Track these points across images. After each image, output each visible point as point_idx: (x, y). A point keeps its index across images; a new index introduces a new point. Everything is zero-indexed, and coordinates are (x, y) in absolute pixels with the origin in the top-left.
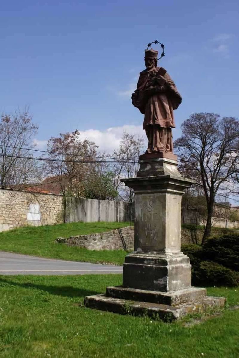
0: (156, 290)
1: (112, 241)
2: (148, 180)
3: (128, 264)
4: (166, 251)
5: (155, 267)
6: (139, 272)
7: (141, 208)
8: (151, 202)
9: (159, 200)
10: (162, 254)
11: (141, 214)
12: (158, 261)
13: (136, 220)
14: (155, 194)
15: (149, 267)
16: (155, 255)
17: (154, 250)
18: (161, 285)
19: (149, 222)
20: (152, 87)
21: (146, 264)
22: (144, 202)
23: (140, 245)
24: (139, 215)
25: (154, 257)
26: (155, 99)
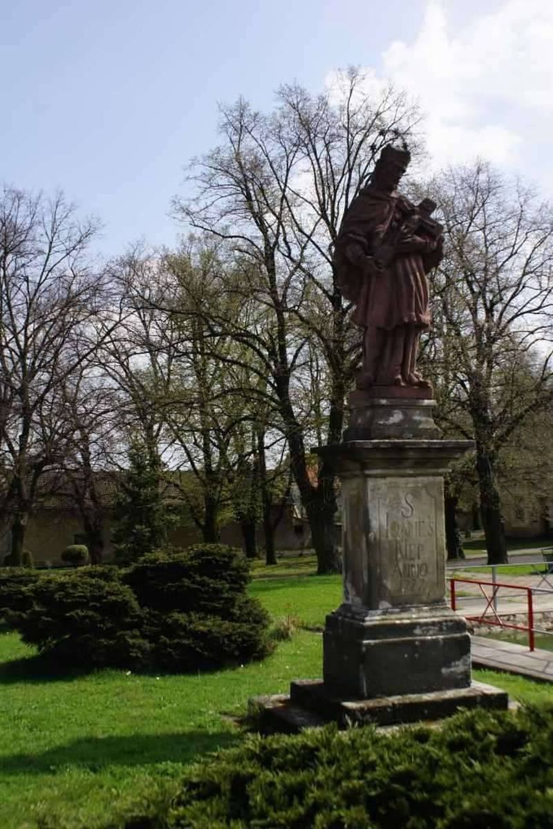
0: (449, 687)
3: (377, 641)
5: (444, 639)
6: (406, 656)
7: (386, 511)
9: (428, 493)
10: (443, 609)
11: (384, 523)
12: (446, 626)
14: (420, 479)
15: (428, 641)
17: (422, 603)
18: (459, 674)
19: (406, 541)
21: (421, 635)
22: (392, 496)
23: (387, 595)
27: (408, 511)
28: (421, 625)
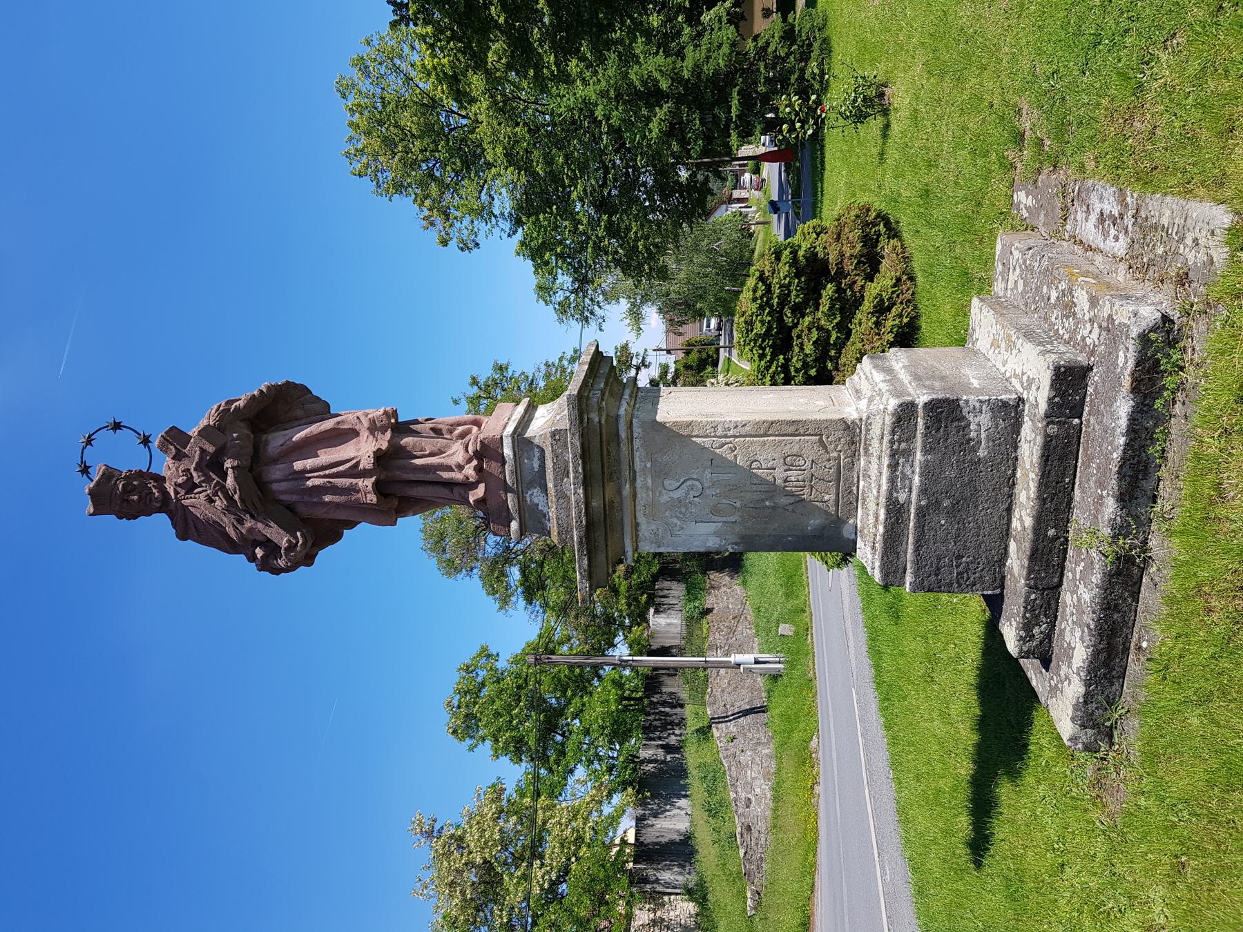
1: (748, 753)
2: (585, 490)
4: (854, 416)
5: (926, 452)
8: (666, 483)
10: (868, 430)
11: (712, 527)
13: (736, 544)
14: (638, 465)
16: (874, 460)
20: (230, 482)
25: (880, 465)
26: (276, 472)
27: (692, 488)
28: (890, 493)
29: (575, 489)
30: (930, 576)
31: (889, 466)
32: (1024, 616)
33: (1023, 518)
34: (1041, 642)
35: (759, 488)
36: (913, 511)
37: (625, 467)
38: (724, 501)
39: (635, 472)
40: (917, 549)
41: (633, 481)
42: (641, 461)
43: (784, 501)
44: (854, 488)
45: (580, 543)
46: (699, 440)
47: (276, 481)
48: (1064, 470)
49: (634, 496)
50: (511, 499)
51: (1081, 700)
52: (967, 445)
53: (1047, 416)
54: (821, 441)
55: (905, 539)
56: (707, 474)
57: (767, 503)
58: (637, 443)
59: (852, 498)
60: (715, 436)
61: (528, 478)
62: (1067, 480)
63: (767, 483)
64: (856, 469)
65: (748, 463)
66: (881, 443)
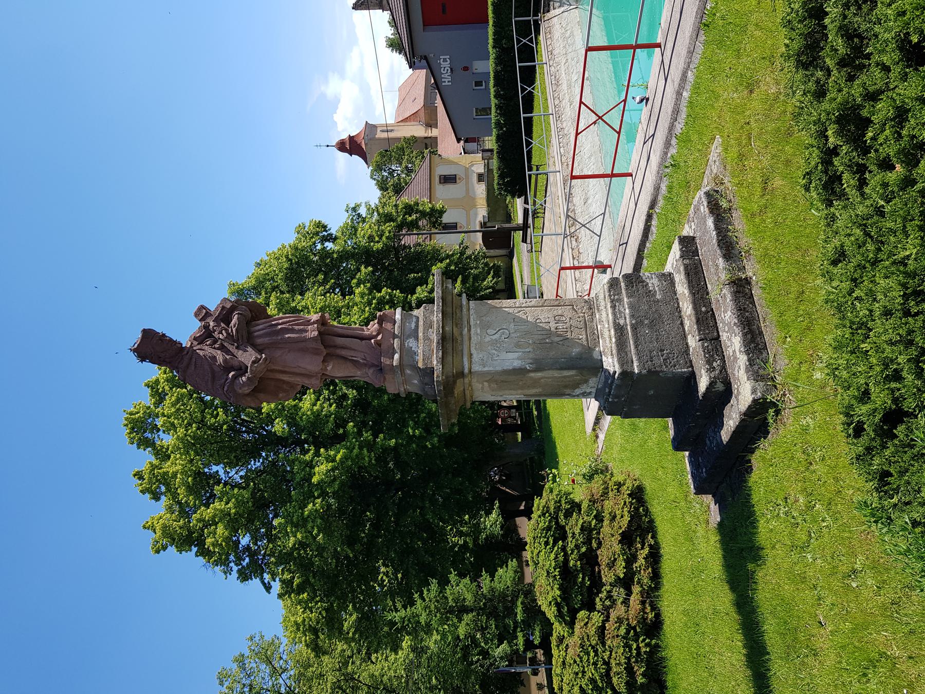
5: (628, 297)
11: (516, 355)
13: (531, 364)
14: (472, 323)
24: (518, 359)
29: (437, 314)
30: (647, 362)
31: (611, 307)
32: (705, 356)
33: (687, 308)
34: (721, 371)
35: (542, 333)
36: (629, 327)
37: (465, 320)
38: (522, 340)
39: (470, 326)
40: (636, 347)
41: (469, 330)
42: (474, 320)
43: (557, 339)
44: (596, 331)
45: (438, 343)
46: (506, 309)
47: (260, 336)
48: (699, 278)
49: (470, 339)
50: (396, 343)
51: (747, 364)
52: (650, 294)
53: (681, 257)
54: (573, 308)
55: (628, 344)
56: (512, 325)
57: (547, 341)
58: (472, 312)
59: (595, 337)
60: (515, 307)
61: (407, 332)
62: (702, 283)
63: (547, 330)
64: (595, 321)
65: (535, 320)
66: (605, 300)
